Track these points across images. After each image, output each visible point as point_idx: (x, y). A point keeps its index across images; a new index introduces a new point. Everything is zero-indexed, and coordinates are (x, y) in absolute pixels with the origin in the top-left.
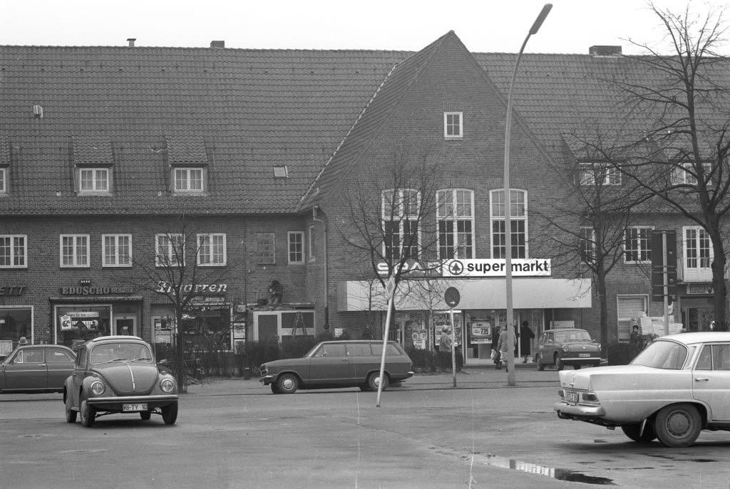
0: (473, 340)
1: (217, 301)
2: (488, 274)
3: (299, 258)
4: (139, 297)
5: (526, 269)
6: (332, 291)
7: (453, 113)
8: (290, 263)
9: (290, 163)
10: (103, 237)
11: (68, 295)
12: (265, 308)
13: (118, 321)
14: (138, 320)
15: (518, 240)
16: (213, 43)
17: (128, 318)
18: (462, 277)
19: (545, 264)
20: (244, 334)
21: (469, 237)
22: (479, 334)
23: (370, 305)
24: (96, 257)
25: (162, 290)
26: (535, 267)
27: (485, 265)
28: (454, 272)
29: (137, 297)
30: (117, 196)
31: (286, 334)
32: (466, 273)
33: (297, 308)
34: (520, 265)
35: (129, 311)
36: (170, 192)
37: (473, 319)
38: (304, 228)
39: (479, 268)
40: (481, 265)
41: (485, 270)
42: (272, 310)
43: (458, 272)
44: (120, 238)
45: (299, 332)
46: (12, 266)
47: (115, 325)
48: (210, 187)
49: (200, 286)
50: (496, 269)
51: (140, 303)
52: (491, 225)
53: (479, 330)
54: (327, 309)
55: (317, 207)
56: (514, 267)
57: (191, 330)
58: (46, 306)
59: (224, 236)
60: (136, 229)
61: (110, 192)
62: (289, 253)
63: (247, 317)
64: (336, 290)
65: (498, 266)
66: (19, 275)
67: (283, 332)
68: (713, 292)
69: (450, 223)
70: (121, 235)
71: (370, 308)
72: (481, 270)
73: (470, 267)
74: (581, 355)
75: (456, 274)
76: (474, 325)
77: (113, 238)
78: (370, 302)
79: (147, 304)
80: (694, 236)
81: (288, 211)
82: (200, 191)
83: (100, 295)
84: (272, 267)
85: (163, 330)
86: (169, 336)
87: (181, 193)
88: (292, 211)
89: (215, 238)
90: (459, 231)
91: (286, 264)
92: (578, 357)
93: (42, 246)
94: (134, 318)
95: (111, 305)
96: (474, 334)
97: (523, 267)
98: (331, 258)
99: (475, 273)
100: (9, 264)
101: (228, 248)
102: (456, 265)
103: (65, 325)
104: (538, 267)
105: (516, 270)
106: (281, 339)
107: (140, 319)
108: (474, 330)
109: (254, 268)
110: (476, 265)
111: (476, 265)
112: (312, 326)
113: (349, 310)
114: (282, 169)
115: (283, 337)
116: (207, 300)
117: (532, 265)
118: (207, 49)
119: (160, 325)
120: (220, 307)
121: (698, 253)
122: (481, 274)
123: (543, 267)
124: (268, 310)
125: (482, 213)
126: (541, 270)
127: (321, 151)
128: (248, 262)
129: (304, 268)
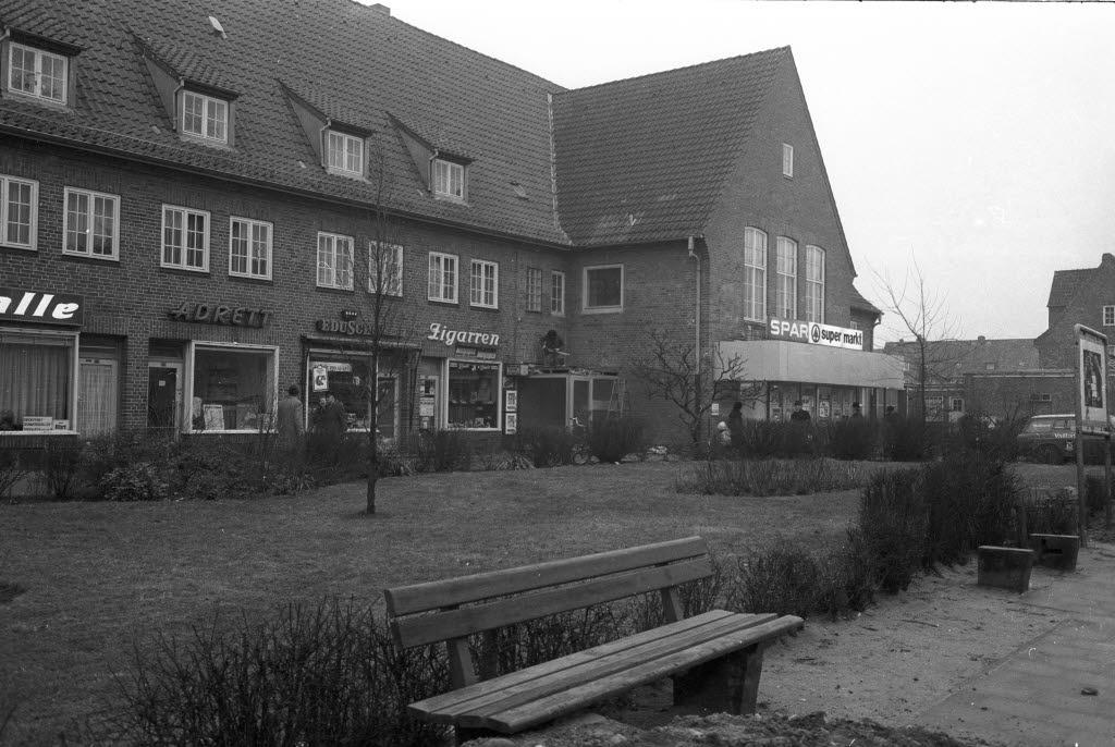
11: (330, 333)
17: (169, 365)
24: (50, 230)
25: (434, 337)
36: (175, 131)
46: (249, 274)
48: (238, 136)
52: (231, 226)
58: (297, 349)
61: (68, 106)
66: (259, 292)
80: (190, 253)
82: (222, 141)
85: (426, 396)
86: (431, 407)
93: (295, 247)
100: (245, 271)
103: (320, 383)
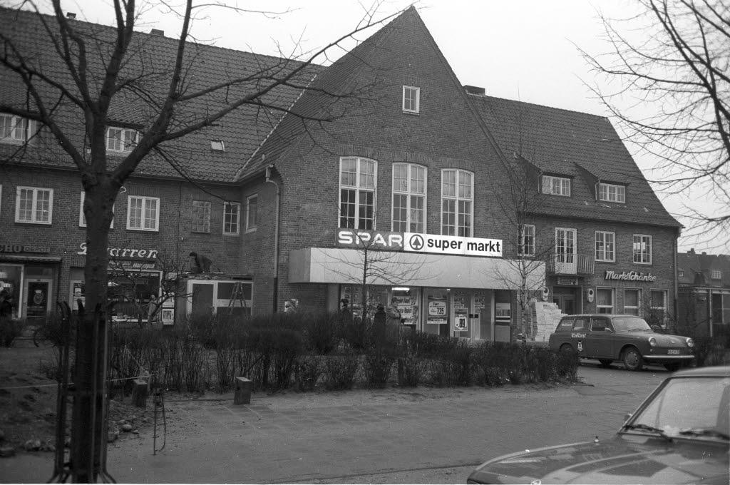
0: (429, 319)
1: (148, 268)
2: (446, 251)
3: (234, 229)
4: (58, 259)
5: (481, 249)
6: (283, 260)
7: (411, 88)
8: (224, 233)
9: (226, 139)
10: (19, 188)
12: (201, 276)
13: (30, 283)
14: (54, 284)
15: (464, 221)
16: (153, 31)
17: (43, 281)
18: (421, 253)
19: (498, 245)
20: (173, 304)
21: (421, 213)
22: (436, 314)
23: (365, 274)
26: (488, 247)
27: (444, 242)
28: (414, 246)
29: (54, 258)
30: (154, 384)
31: (222, 305)
32: (426, 249)
33: (235, 279)
34: (475, 244)
35: (40, 273)
37: (430, 298)
38: (241, 200)
39: (438, 245)
40: (440, 241)
41: (444, 247)
42: (209, 279)
43: (419, 247)
44: (40, 193)
45: (237, 304)
47: (27, 288)
49: (129, 250)
50: (454, 246)
51: (57, 265)
53: (436, 309)
54: (276, 280)
55: (272, 166)
56: (470, 245)
57: (115, 297)
59: (158, 200)
60: (59, 184)
62: (224, 223)
63: (176, 287)
64: (288, 260)
65: (456, 244)
67: (218, 303)
68: (577, 284)
69: (404, 197)
70: (41, 189)
71: (364, 281)
72: (440, 247)
73: (430, 243)
74: (670, 351)
75: (417, 249)
76: (431, 304)
77: (31, 192)
78: (365, 270)
79: (66, 267)
81: (226, 180)
83: (10, 253)
84: (206, 236)
87: (114, 152)
88: (230, 181)
89: (148, 201)
90: (411, 207)
91: (221, 235)
92: (666, 354)
94: (50, 282)
95: (23, 267)
96: (431, 313)
97: (478, 246)
98: (285, 224)
99: (434, 250)
101: (161, 213)
102: (417, 239)
104: (492, 248)
105: (472, 249)
106: (216, 309)
107: (56, 282)
108: (430, 309)
109: (187, 235)
110: (436, 241)
111: (436, 241)
112: (250, 299)
113: (313, 280)
114: (219, 143)
115: (218, 308)
116: (135, 265)
117: (487, 245)
118: (147, 35)
119: (80, 290)
120: (148, 275)
121: (565, 249)
122: (439, 250)
123: (495, 247)
124: (203, 279)
125: (434, 190)
126: (494, 251)
127: (255, 133)
128: (181, 228)
129: (238, 241)
